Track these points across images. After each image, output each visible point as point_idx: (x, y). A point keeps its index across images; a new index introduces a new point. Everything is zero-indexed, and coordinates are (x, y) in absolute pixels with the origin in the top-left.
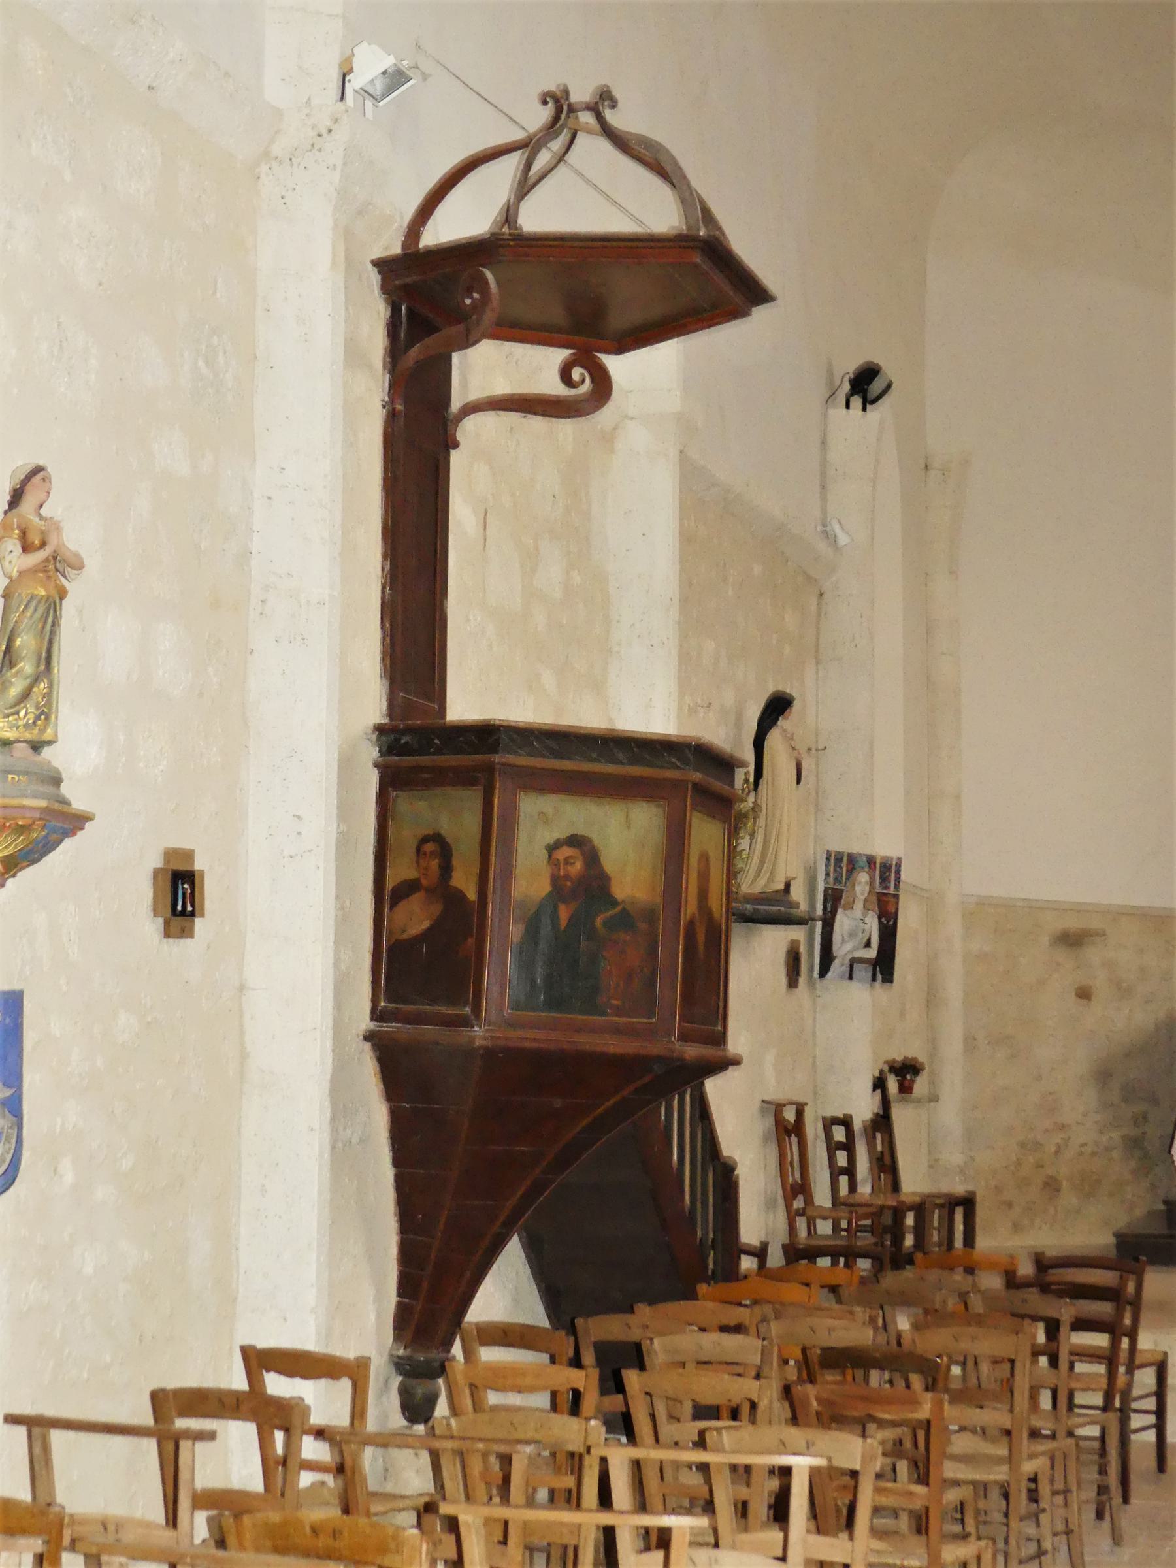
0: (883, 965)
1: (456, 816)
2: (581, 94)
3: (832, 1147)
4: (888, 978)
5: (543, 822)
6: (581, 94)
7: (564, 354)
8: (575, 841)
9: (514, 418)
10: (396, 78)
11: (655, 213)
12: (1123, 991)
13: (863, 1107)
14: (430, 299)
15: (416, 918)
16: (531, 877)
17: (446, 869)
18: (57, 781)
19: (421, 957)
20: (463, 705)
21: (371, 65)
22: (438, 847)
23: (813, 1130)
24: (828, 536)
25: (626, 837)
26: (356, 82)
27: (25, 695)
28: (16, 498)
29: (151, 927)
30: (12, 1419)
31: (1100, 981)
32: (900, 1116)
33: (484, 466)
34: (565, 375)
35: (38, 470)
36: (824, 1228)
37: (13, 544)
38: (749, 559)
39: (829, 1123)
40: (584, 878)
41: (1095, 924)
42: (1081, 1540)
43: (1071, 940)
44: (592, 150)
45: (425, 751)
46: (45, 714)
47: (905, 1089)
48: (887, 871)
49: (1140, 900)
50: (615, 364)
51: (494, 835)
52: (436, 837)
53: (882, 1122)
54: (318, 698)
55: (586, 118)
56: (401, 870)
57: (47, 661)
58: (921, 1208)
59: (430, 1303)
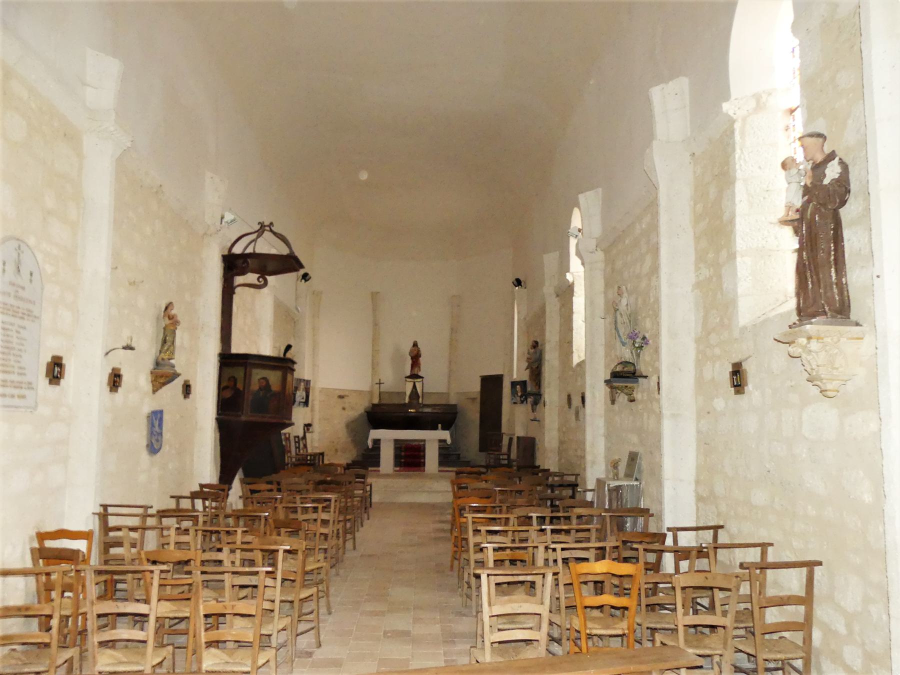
0: (306, 403)
1: (239, 373)
2: (267, 223)
3: (296, 442)
4: (307, 406)
5: (258, 374)
6: (267, 223)
7: (257, 275)
8: (263, 378)
9: (247, 288)
10: (233, 221)
11: (285, 251)
12: (352, 408)
13: (301, 435)
14: (233, 265)
15: (228, 394)
16: (255, 386)
17: (235, 384)
18: (174, 367)
19: (228, 402)
20: (234, 350)
21: (229, 217)
22: (234, 379)
23: (292, 438)
24: (297, 309)
25: (274, 377)
26: (225, 220)
27: (168, 350)
28: (166, 308)
29: (182, 397)
30: (172, 497)
31: (346, 406)
32: (307, 434)
33: (241, 297)
34: (258, 279)
35: (171, 303)
36: (294, 460)
37: (167, 319)
38: (286, 317)
39: (295, 437)
40: (266, 386)
41: (347, 393)
42: (94, 657)
43: (341, 397)
44: (267, 234)
45: (229, 361)
46: (173, 353)
47: (308, 430)
48: (308, 382)
49: (355, 389)
50: (269, 278)
51: (247, 377)
52: (234, 377)
53: (304, 437)
54: (212, 349)
55: (268, 228)
56: (224, 384)
57: (173, 342)
58: (311, 455)
59: (226, 477)
